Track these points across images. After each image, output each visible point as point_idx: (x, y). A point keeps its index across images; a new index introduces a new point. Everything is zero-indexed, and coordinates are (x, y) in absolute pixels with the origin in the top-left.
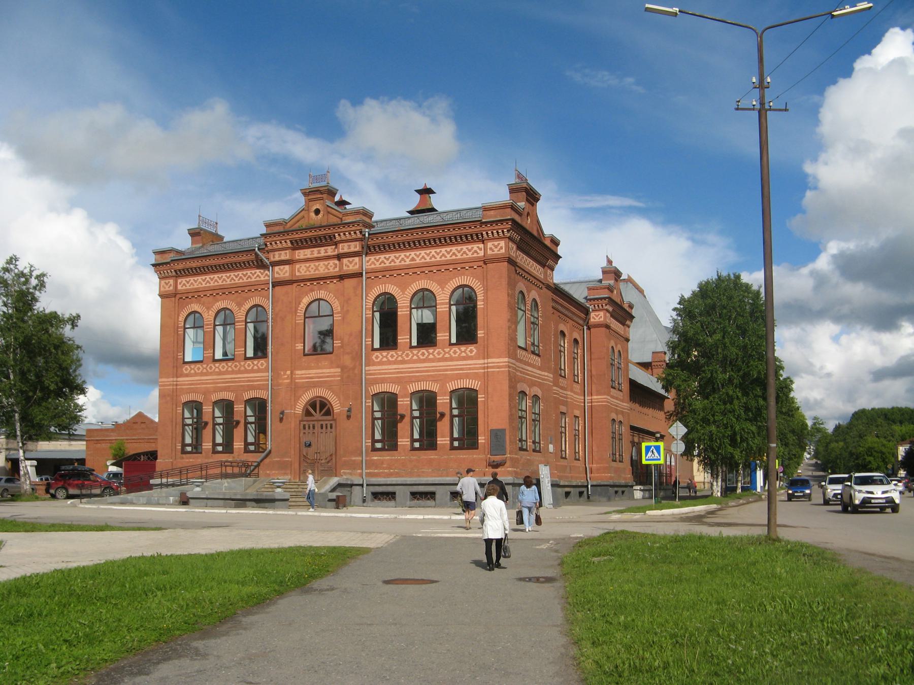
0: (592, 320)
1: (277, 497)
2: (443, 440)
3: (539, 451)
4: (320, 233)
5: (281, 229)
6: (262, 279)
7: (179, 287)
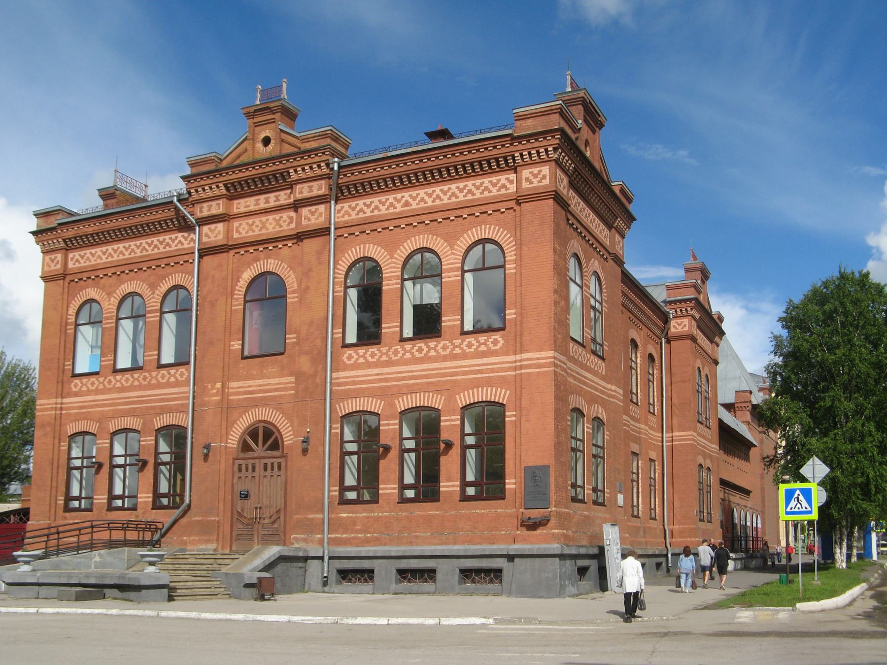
0: (673, 330)
1: (144, 582)
2: (449, 486)
3: (602, 504)
4: (268, 169)
5: (212, 167)
6: (186, 246)
7: (71, 265)
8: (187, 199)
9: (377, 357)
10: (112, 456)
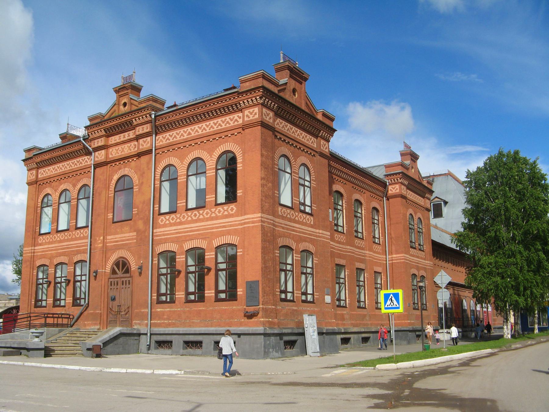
0: (390, 192)
1: (30, 347)
4: (123, 120)
7: (40, 176)
8: (88, 138)
9: (209, 215)
10: (75, 276)
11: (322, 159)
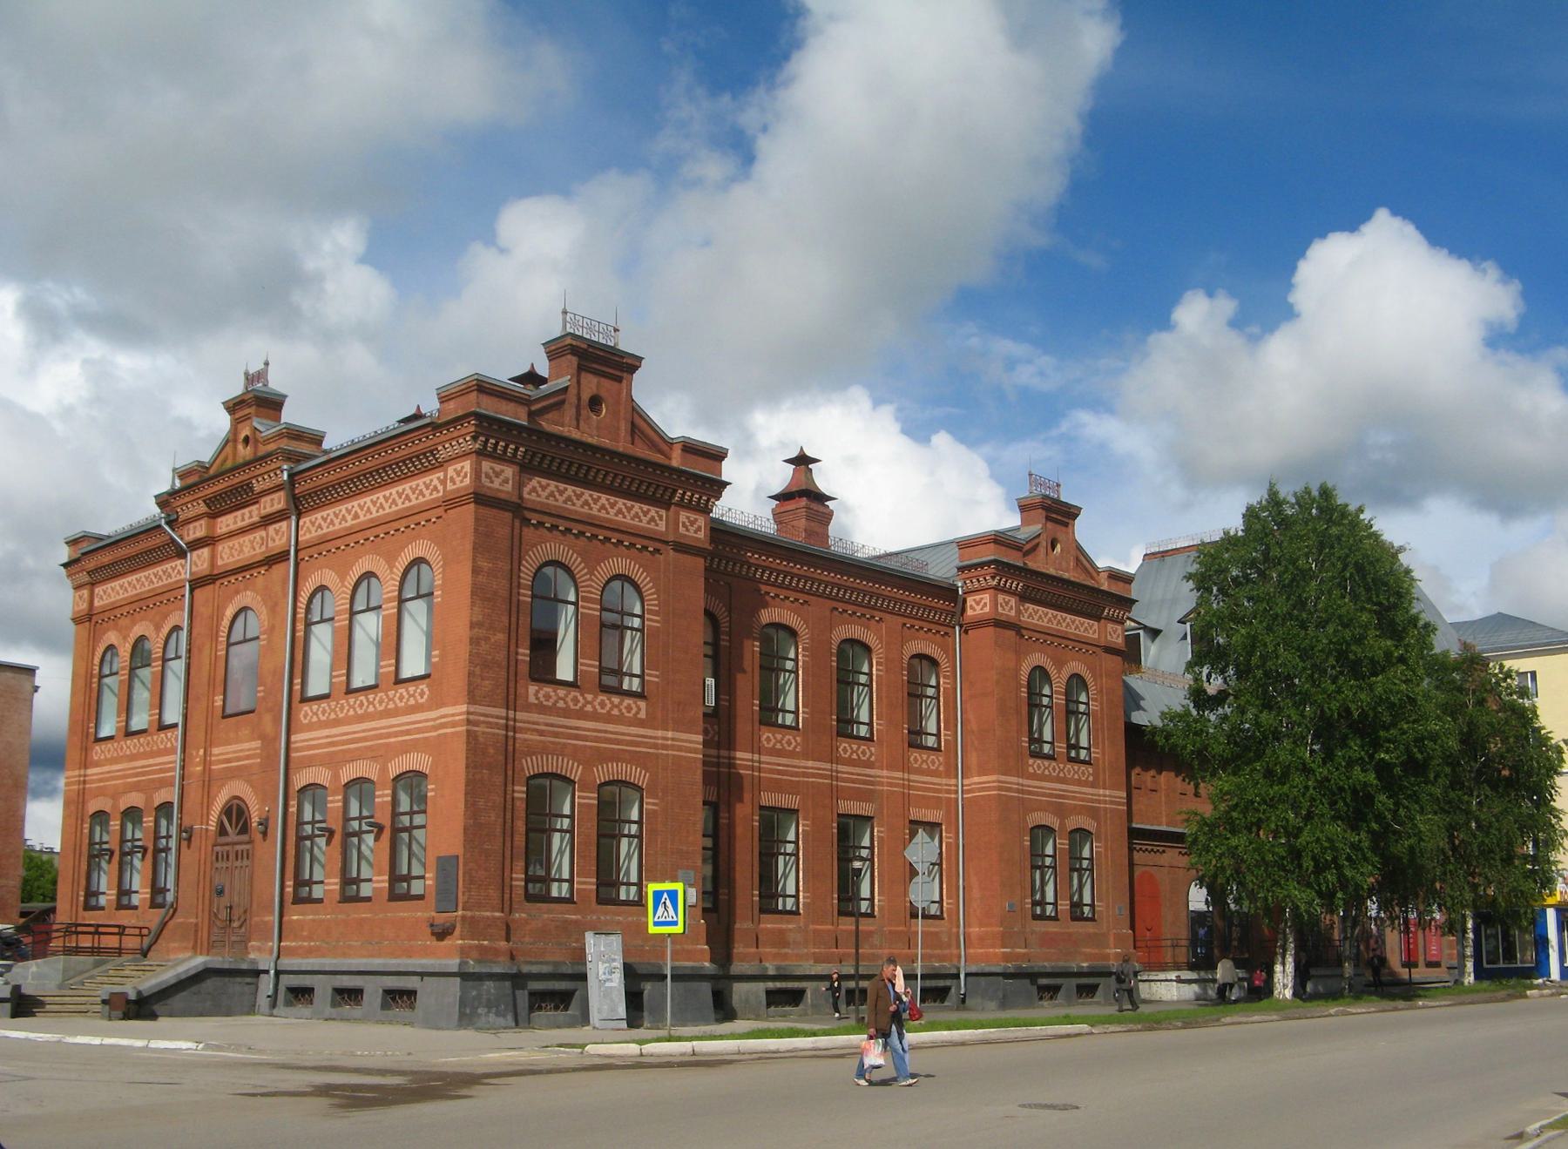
0: (969, 612)
7: (96, 603)
11: (681, 556)
